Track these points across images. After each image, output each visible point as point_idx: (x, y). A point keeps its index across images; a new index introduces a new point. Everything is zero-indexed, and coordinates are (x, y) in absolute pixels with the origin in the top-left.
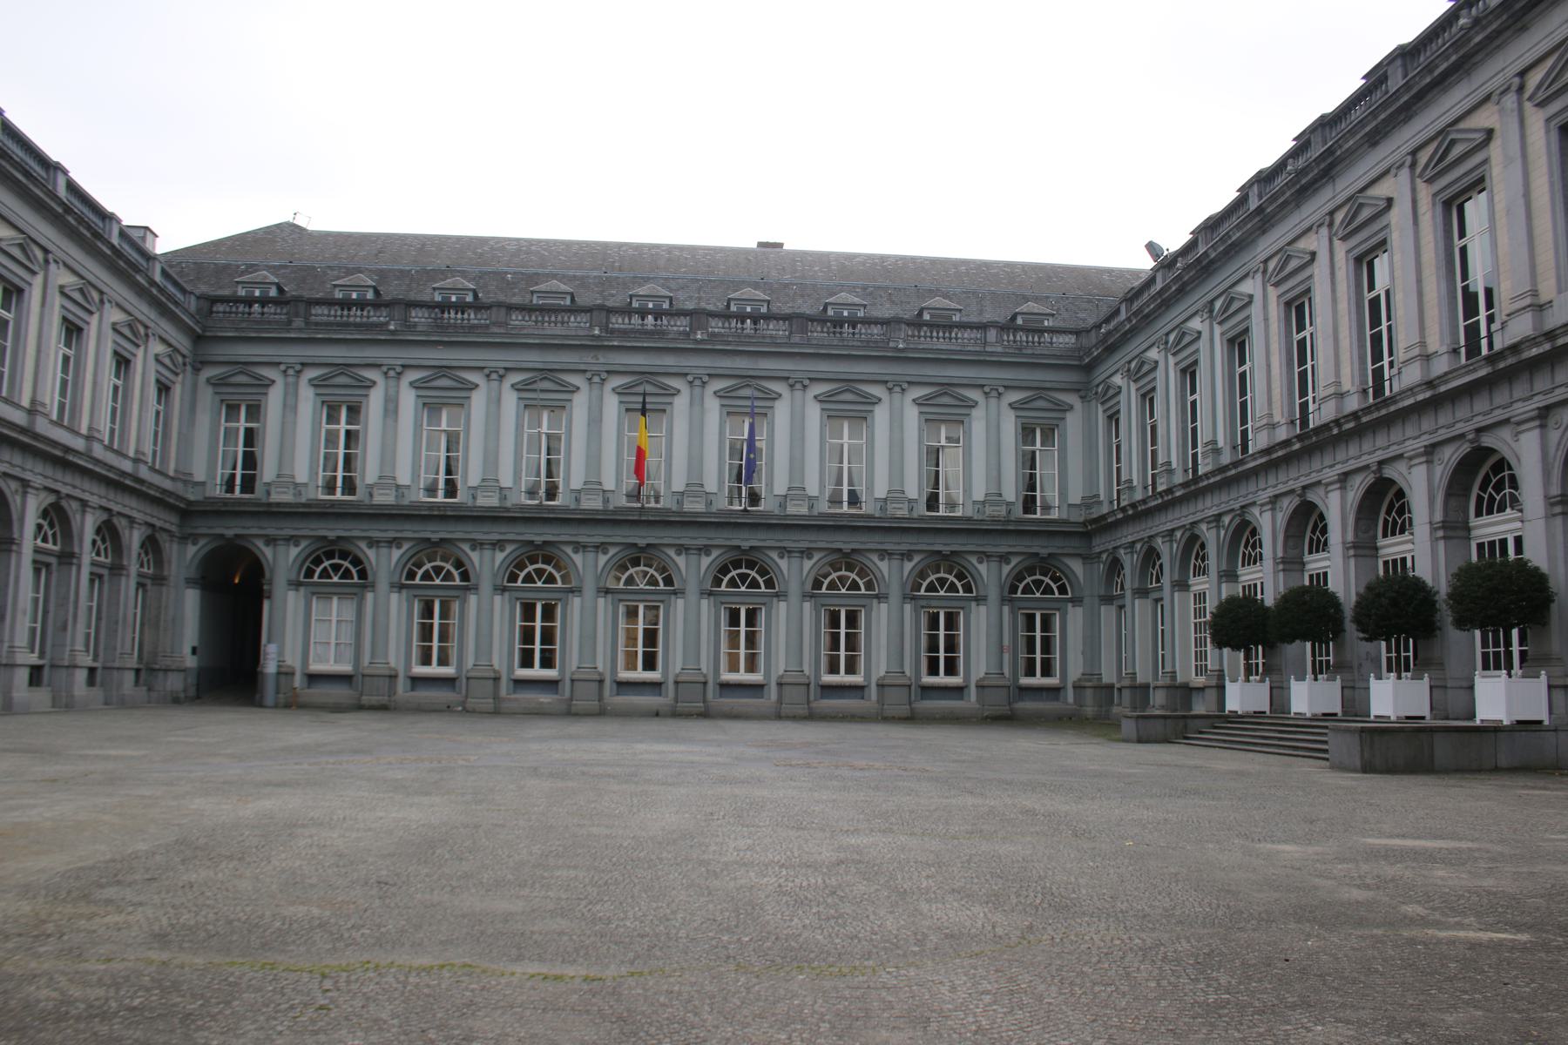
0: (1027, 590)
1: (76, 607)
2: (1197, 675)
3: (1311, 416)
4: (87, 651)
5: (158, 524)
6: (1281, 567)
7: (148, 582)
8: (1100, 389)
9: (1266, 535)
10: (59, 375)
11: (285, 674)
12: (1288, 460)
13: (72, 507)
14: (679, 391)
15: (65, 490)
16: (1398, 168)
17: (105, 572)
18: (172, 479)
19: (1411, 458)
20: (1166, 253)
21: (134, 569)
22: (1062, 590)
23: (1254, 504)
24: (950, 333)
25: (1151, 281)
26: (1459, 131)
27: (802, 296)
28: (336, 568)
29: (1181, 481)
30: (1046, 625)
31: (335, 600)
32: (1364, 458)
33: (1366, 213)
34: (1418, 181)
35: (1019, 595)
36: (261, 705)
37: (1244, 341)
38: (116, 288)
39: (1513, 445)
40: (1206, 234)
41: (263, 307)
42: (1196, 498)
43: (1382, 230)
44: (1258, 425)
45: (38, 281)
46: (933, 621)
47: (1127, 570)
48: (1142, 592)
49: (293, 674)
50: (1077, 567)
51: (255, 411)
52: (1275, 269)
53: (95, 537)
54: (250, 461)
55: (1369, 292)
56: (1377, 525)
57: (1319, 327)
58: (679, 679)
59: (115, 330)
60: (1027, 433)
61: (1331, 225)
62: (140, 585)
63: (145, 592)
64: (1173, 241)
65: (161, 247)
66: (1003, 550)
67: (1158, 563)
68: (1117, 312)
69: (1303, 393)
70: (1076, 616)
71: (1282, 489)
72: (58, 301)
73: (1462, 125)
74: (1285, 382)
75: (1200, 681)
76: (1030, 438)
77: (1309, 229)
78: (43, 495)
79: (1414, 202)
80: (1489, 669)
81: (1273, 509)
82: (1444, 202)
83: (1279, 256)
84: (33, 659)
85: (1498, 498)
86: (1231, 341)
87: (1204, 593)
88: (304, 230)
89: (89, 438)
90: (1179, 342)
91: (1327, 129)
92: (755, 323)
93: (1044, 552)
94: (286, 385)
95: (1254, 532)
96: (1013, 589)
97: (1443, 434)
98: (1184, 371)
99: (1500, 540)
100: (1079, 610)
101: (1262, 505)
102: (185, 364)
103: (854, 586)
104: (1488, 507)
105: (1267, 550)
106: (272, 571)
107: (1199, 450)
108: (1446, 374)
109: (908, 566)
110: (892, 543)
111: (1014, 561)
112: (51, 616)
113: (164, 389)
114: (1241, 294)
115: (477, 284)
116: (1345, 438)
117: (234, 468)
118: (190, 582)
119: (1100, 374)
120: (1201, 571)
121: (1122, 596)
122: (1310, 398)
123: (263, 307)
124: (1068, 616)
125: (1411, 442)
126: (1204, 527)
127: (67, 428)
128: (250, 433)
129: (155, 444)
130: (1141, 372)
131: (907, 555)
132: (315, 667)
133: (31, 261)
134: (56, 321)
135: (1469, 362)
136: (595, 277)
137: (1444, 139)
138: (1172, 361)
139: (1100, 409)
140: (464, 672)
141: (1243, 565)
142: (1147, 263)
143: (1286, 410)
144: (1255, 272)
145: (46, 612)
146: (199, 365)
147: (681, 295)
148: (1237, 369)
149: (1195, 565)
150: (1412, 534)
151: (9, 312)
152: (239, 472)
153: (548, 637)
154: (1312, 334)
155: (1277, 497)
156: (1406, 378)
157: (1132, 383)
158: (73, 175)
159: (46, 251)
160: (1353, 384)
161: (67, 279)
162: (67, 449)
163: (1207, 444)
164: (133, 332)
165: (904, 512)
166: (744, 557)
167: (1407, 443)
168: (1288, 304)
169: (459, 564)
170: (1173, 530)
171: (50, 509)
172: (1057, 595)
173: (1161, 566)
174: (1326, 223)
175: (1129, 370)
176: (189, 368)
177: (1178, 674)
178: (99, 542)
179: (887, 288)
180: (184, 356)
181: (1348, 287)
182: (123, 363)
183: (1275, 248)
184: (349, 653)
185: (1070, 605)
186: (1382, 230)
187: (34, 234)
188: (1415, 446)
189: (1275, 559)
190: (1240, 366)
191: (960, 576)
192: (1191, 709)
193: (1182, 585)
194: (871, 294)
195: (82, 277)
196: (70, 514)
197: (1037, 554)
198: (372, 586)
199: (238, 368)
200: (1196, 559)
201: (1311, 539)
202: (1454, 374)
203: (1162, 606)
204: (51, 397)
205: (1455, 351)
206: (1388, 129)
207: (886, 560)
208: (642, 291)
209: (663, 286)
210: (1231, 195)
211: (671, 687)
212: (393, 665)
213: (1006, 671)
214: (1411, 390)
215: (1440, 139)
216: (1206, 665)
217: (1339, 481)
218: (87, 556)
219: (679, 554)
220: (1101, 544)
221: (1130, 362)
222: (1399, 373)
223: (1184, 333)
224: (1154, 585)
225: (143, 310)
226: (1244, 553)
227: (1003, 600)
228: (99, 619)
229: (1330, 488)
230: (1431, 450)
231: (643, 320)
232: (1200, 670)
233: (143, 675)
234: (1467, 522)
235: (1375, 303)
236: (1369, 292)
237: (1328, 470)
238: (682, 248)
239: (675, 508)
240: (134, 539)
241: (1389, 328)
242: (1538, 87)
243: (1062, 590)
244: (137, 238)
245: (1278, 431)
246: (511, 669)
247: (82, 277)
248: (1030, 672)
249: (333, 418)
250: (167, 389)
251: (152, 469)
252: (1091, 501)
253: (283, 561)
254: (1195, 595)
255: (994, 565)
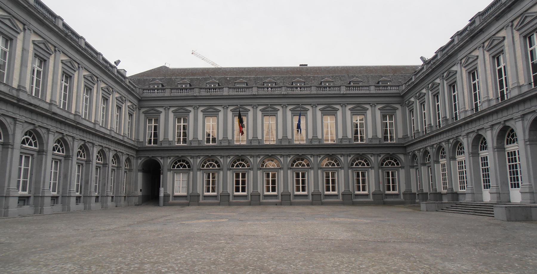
0: (387, 164)
1: (108, 179)
2: (444, 190)
3: (479, 107)
4: (111, 192)
5: (130, 154)
6: (471, 155)
7: (128, 171)
8: (407, 103)
9: (465, 145)
10: (102, 113)
11: (166, 196)
12: (471, 122)
13: (106, 150)
14: (279, 110)
15: (104, 146)
16: (479, 48)
17: (116, 169)
18: (134, 141)
19: (516, 119)
20: (427, 59)
21: (123, 167)
22: (398, 164)
23: (461, 135)
24: (359, 88)
25: (423, 68)
26: (528, 13)
27: (314, 80)
28: (181, 165)
29: (422, 135)
30: (303, 176)
31: (181, 174)
32: (498, 120)
33: (496, 42)
34: (514, 30)
35: (294, 167)
36: (159, 206)
37: (454, 85)
38: (117, 87)
39: (515, 125)
40: (480, 18)
41: (158, 91)
42: (452, 130)
43: (501, 47)
44: (460, 111)
45: (95, 86)
46: (358, 176)
47: (418, 158)
48: (424, 164)
49: (170, 196)
50: (402, 157)
51: (157, 121)
52: (464, 62)
53: (98, 155)
54: (156, 135)
55: (498, 67)
56: (504, 141)
57: (481, 79)
58: (282, 194)
59: (116, 99)
60: (384, 117)
61: (483, 47)
62: (125, 172)
63: (127, 174)
64: (429, 56)
65: (128, 75)
66: (379, 152)
67: (429, 155)
68: (411, 79)
69: (476, 100)
70: (402, 172)
71: (470, 131)
72: (101, 91)
73: (529, 11)
74: (469, 97)
75: (445, 191)
76: (385, 118)
77: (476, 49)
78: (98, 147)
79: (513, 37)
80: (513, 188)
81: (467, 137)
82: (492, 57)
83: (466, 58)
84: (78, 194)
85: (512, 139)
86: (450, 85)
87: (445, 164)
88: (169, 68)
89: (95, 124)
90: (432, 87)
91: (481, 16)
92: (301, 89)
93: (391, 153)
94: (165, 113)
95: (461, 144)
96: (382, 164)
97: (527, 111)
98: (434, 96)
99: (514, 151)
100: (373, 171)
101: (463, 136)
102: (136, 108)
103: (333, 165)
104: (510, 142)
105: (466, 150)
106: (163, 167)
107: (427, 126)
108: (527, 92)
109: (349, 158)
110: (344, 152)
111: (382, 156)
112: (101, 181)
113: (131, 115)
114: (453, 71)
115: (219, 81)
116: (492, 114)
117: (151, 137)
118: (139, 171)
119: (407, 97)
120: (442, 157)
121: (417, 166)
122: (478, 101)
123: (158, 91)
124: (400, 172)
125: (515, 114)
126: (416, 152)
127: (87, 120)
128: (155, 127)
129: (129, 131)
130: (421, 97)
131: (349, 155)
132: (176, 194)
133: (49, 50)
134: (83, 86)
135: (536, 87)
136: (253, 77)
137: (523, 16)
138: (445, 82)
139: (407, 109)
140: (219, 194)
141: (458, 155)
142: (421, 63)
143: (470, 106)
144: (457, 63)
145: (99, 181)
146: (140, 108)
147: (278, 82)
148: (452, 94)
149: (441, 155)
150: (518, 143)
151: (41, 69)
152: (152, 138)
153: (244, 182)
154: (478, 82)
155: (493, 125)
156: (483, 106)
157: (417, 100)
158: (87, 40)
159: (97, 78)
160: (493, 97)
161: (103, 85)
162: (105, 134)
163: (429, 125)
164: (121, 100)
165: (347, 143)
166: (300, 158)
167: (514, 114)
168: (469, 73)
169: (217, 162)
170: (420, 149)
171: (82, 146)
172: (396, 166)
173: (430, 156)
174: (482, 47)
175: (416, 96)
176: (137, 109)
177: (454, 189)
178: (114, 160)
179: (339, 76)
180: (136, 106)
181: (490, 66)
182: (119, 108)
183: (446, 69)
184: (185, 189)
185: (400, 169)
186: (501, 47)
187: (48, 39)
188: (517, 115)
189: (469, 153)
190: (453, 93)
191: (366, 161)
192: (442, 200)
193: (437, 162)
194: (334, 78)
195: (107, 85)
196: (106, 152)
197: (389, 154)
198: (192, 170)
199: (152, 108)
200: (441, 153)
201: (481, 146)
202: (531, 91)
203: (431, 168)
204: (100, 120)
205: (530, 84)
206: (502, 15)
207: (343, 157)
208: (267, 81)
209: (273, 79)
210: (449, 40)
211: (402, 195)
212: (198, 193)
213: (381, 190)
214: (515, 97)
215: (521, 16)
216: (447, 187)
217: (490, 127)
218: (111, 164)
219: (191, 159)
220: (409, 150)
221: (416, 94)
222: (510, 92)
223: (434, 84)
224: (428, 162)
225: (124, 93)
226: (458, 151)
227: (379, 168)
228: (114, 182)
229: (487, 130)
230: (523, 116)
231: (268, 89)
232: (445, 188)
233: (126, 198)
234: (439, 161)
235: (500, 71)
236: (498, 67)
237: (486, 124)
238: (278, 68)
239: (279, 144)
240: (123, 158)
241: (506, 78)
242: (464, 63)
243: (398, 164)
244: (121, 74)
245: (468, 112)
246: (293, 192)
247: (107, 85)
248: (328, 190)
249: (179, 122)
250: (132, 115)
251: (128, 138)
252: (405, 137)
253: (166, 163)
254: (442, 165)
255: (376, 157)
